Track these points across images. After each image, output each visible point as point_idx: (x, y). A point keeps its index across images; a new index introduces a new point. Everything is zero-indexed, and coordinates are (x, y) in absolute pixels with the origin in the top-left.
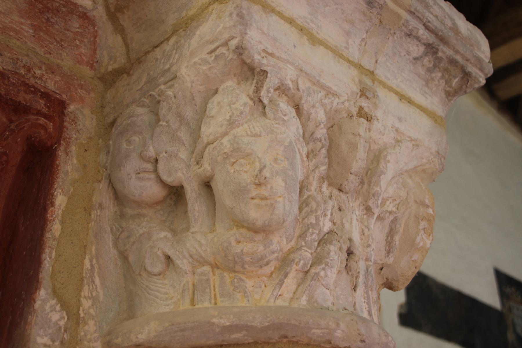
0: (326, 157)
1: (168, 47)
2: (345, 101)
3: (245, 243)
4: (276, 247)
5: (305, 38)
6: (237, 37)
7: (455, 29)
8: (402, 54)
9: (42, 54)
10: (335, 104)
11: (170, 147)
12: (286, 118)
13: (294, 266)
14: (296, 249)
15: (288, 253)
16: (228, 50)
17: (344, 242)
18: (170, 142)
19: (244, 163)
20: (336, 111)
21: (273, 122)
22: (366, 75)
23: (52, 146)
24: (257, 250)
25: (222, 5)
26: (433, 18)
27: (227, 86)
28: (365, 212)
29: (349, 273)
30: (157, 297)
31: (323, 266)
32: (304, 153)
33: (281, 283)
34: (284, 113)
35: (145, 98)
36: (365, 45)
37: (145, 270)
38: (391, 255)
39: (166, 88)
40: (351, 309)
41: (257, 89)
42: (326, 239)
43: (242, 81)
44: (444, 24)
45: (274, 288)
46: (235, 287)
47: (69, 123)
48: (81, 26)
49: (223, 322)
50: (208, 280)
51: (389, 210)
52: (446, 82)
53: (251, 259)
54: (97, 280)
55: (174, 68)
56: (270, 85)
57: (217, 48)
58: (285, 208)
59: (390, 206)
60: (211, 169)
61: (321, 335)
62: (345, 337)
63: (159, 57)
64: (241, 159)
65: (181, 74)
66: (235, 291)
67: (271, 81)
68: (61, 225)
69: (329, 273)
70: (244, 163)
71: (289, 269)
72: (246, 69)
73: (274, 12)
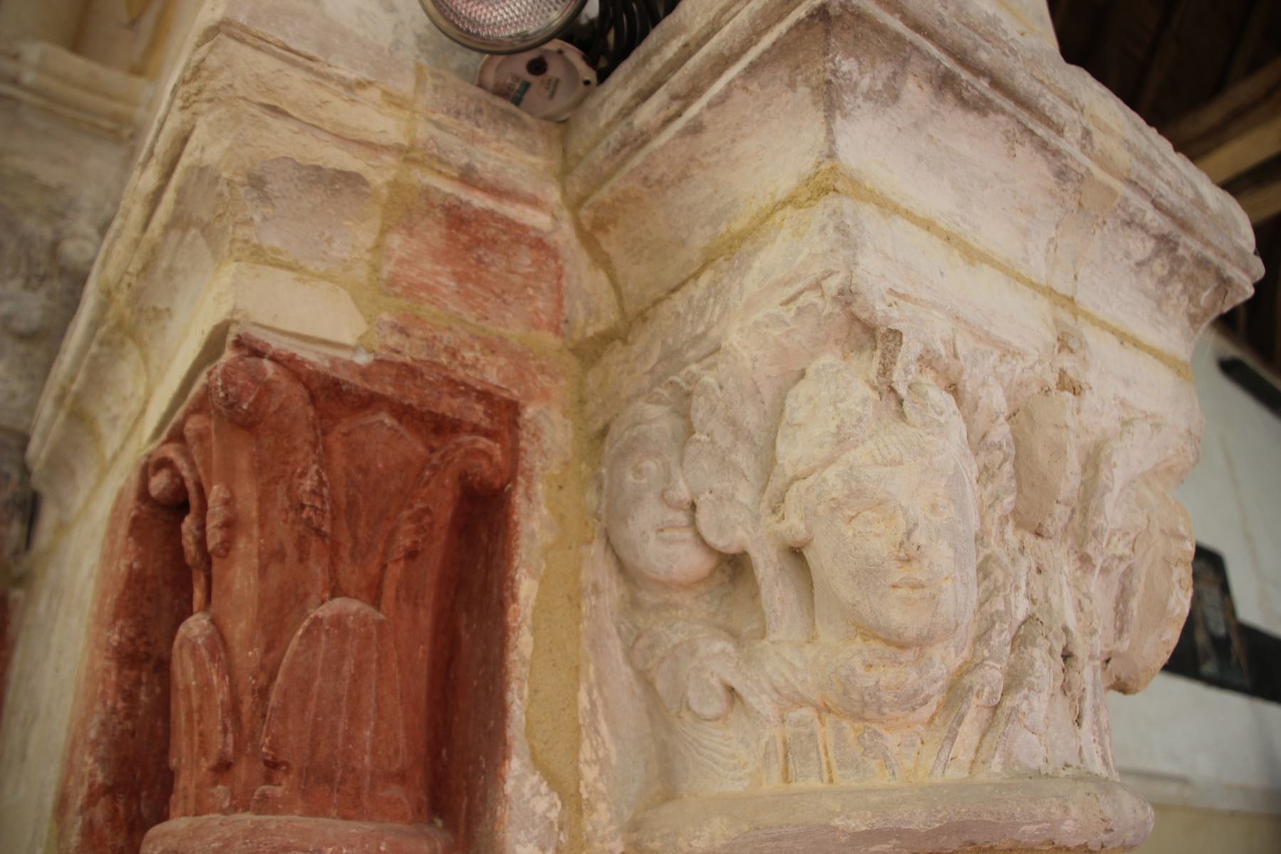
0: (1012, 478)
1: (697, 290)
2: (1035, 364)
3: (882, 669)
4: (940, 669)
5: (957, 252)
6: (838, 272)
7: (1199, 203)
8: (1117, 258)
9: (473, 321)
10: (1018, 371)
11: (719, 482)
12: (942, 419)
13: (974, 699)
14: (973, 666)
15: (958, 674)
16: (823, 295)
17: (1056, 638)
18: (717, 472)
19: (874, 518)
20: (1021, 384)
21: (921, 432)
22: (1063, 306)
23: (503, 487)
24: (907, 680)
25: (802, 211)
26: (1166, 187)
27: (823, 365)
28: (1078, 564)
29: (1067, 693)
30: (717, 763)
31: (1025, 691)
32: (974, 475)
33: (952, 737)
34: (938, 410)
35: (661, 387)
36: (1055, 250)
37: (689, 708)
38: (1126, 635)
39: (702, 369)
40: (1074, 761)
41: (884, 369)
42: (1023, 635)
43: (852, 351)
44: (1181, 195)
45: (940, 747)
46: (865, 749)
47: (528, 440)
48: (534, 262)
49: (854, 825)
50: (812, 735)
51: (1119, 553)
52: (1191, 299)
53: (896, 697)
54: (604, 728)
55: (714, 333)
56: (910, 358)
57: (801, 293)
58: (956, 600)
59: (1121, 548)
60: (806, 528)
61: (1037, 833)
62: (1079, 831)
63: (681, 310)
64: (864, 510)
65: (731, 345)
66: (866, 756)
67: (910, 350)
68: (532, 635)
69: (1035, 703)
70: (874, 518)
71: (965, 706)
72: (857, 329)
73: (898, 213)
